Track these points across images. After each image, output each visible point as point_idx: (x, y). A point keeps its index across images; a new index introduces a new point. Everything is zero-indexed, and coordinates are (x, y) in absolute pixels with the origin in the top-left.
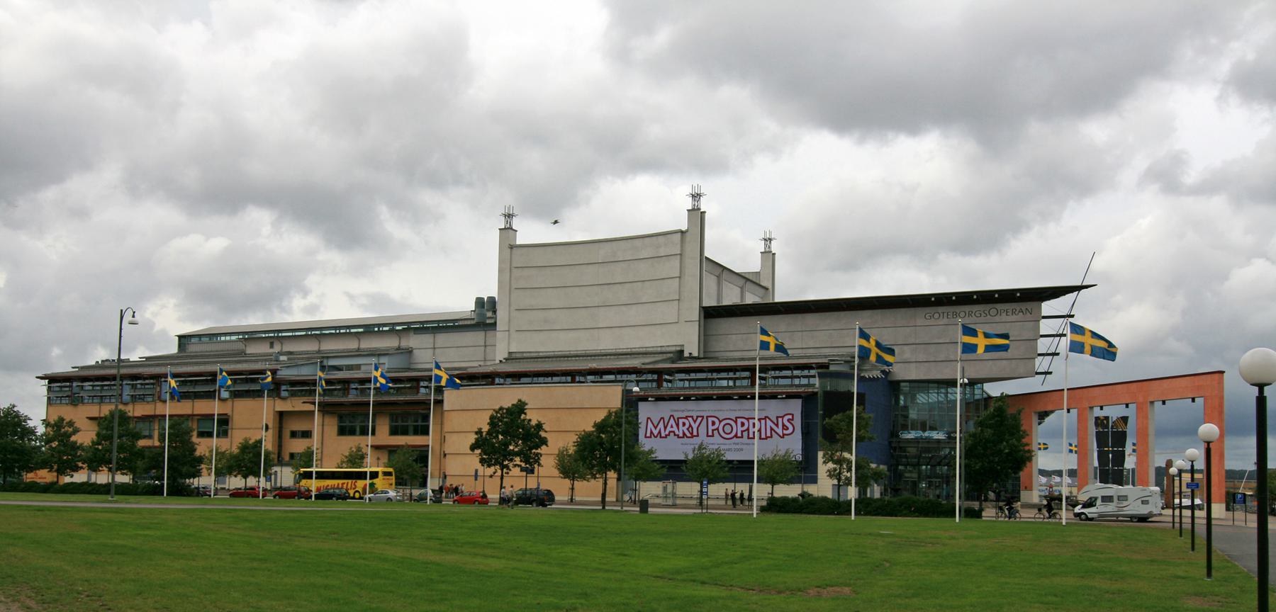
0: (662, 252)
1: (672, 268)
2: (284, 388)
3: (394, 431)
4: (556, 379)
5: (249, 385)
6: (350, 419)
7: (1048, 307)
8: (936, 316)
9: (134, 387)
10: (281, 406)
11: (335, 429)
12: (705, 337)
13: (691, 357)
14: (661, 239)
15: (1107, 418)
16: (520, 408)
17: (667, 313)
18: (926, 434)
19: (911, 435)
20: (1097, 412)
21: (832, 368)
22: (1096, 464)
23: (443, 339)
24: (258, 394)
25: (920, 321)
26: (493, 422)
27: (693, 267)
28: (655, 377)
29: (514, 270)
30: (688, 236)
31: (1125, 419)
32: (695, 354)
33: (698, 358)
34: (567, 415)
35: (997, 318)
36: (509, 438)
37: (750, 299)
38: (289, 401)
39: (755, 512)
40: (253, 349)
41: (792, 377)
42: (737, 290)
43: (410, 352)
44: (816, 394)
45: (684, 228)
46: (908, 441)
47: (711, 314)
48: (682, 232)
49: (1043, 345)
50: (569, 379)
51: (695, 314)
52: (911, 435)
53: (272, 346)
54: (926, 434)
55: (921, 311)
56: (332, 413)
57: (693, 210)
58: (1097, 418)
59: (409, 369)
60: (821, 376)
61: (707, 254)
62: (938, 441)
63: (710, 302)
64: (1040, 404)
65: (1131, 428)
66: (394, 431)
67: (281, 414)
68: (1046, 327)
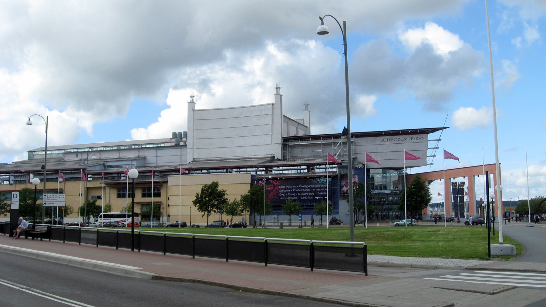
0: (264, 113)
1: (269, 120)
2: (89, 176)
3: (144, 195)
4: (219, 171)
5: (73, 174)
6: (122, 188)
7: (431, 136)
8: (385, 140)
9: (15, 176)
10: (89, 185)
11: (116, 195)
13: (278, 160)
14: (263, 107)
15: (456, 183)
16: (215, 185)
17: (268, 140)
18: (382, 191)
19: (376, 192)
20: (452, 180)
21: (343, 164)
22: (453, 201)
23: (160, 152)
24: (78, 179)
25: (378, 143)
26: (203, 190)
27: (278, 120)
28: (264, 169)
29: (195, 122)
30: (275, 106)
31: (463, 183)
32: (280, 158)
33: (281, 160)
34: (236, 187)
35: (410, 141)
36: (210, 199)
37: (301, 133)
38: (91, 182)
39: (328, 224)
40: (67, 158)
41: (290, 170)
42: (295, 128)
43: (144, 158)
44: (337, 176)
45: (273, 103)
46: (375, 195)
48: (272, 104)
49: (429, 152)
50: (225, 170)
51: (279, 141)
52: (376, 192)
53: (77, 156)
54: (382, 191)
55: (378, 138)
56: (113, 188)
57: (277, 94)
58: (453, 183)
59: (145, 167)
60: (339, 168)
61: (283, 114)
62: (387, 194)
63: (285, 135)
64: (430, 177)
65: (466, 185)
66: (144, 195)
67: (88, 189)
68: (430, 144)
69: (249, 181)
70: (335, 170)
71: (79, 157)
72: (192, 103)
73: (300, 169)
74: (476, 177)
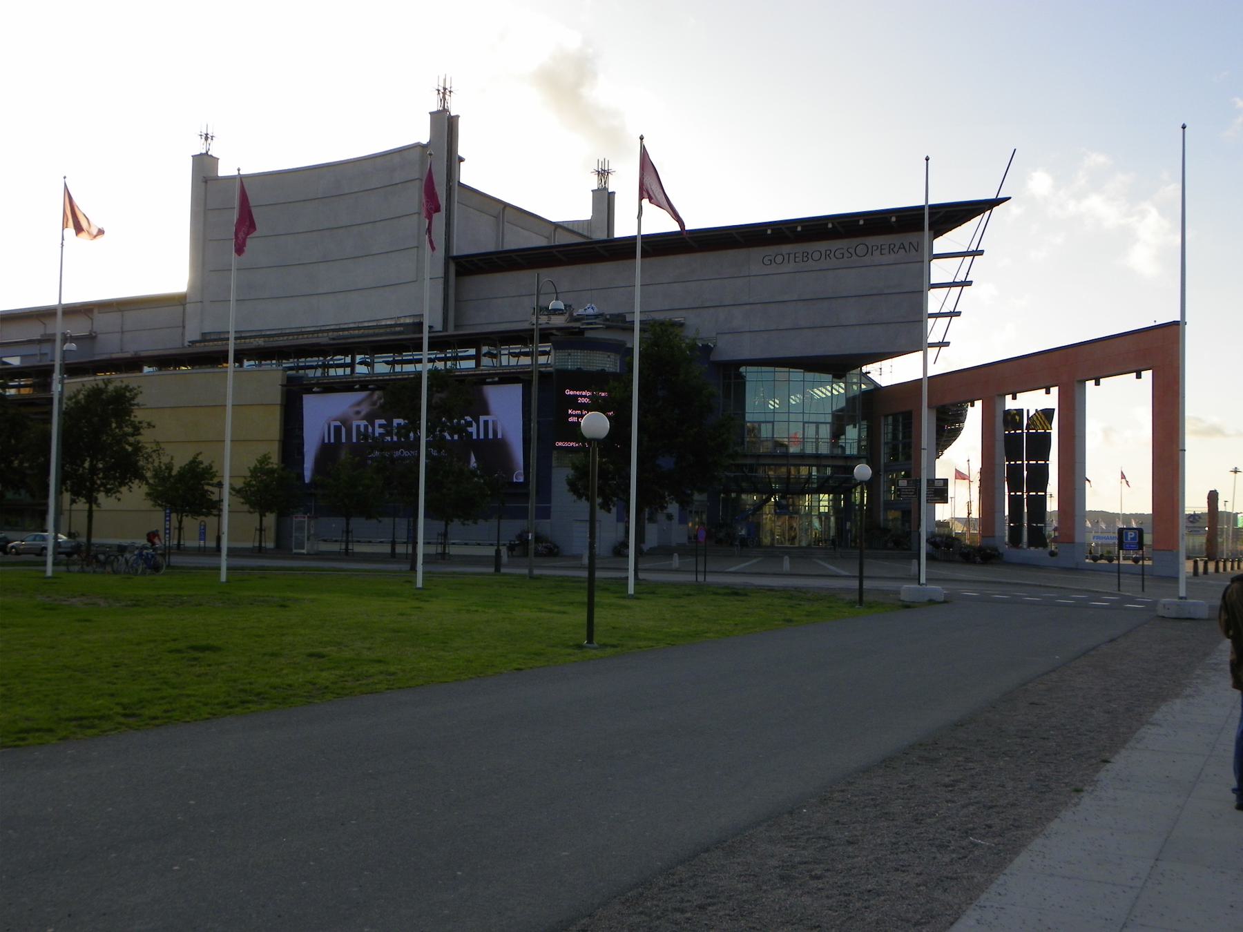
12: (452, 302)
47: (466, 267)
55: (758, 253)
68: (940, 271)
69: (276, 396)
72: (204, 166)
73: (456, 358)
74: (1090, 384)
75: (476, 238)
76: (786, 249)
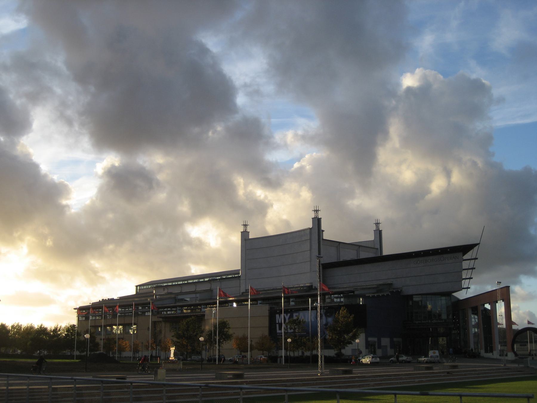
12: (324, 279)
47: (326, 267)
68: (465, 265)
70: (342, 300)
71: (166, 291)
72: (245, 235)
75: (330, 257)
76: (445, 256)
